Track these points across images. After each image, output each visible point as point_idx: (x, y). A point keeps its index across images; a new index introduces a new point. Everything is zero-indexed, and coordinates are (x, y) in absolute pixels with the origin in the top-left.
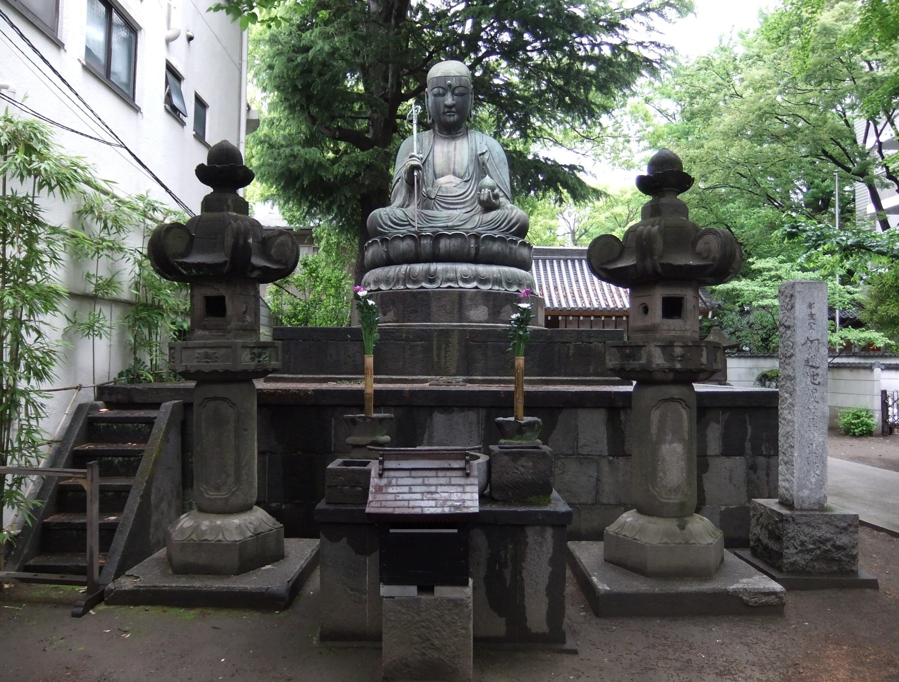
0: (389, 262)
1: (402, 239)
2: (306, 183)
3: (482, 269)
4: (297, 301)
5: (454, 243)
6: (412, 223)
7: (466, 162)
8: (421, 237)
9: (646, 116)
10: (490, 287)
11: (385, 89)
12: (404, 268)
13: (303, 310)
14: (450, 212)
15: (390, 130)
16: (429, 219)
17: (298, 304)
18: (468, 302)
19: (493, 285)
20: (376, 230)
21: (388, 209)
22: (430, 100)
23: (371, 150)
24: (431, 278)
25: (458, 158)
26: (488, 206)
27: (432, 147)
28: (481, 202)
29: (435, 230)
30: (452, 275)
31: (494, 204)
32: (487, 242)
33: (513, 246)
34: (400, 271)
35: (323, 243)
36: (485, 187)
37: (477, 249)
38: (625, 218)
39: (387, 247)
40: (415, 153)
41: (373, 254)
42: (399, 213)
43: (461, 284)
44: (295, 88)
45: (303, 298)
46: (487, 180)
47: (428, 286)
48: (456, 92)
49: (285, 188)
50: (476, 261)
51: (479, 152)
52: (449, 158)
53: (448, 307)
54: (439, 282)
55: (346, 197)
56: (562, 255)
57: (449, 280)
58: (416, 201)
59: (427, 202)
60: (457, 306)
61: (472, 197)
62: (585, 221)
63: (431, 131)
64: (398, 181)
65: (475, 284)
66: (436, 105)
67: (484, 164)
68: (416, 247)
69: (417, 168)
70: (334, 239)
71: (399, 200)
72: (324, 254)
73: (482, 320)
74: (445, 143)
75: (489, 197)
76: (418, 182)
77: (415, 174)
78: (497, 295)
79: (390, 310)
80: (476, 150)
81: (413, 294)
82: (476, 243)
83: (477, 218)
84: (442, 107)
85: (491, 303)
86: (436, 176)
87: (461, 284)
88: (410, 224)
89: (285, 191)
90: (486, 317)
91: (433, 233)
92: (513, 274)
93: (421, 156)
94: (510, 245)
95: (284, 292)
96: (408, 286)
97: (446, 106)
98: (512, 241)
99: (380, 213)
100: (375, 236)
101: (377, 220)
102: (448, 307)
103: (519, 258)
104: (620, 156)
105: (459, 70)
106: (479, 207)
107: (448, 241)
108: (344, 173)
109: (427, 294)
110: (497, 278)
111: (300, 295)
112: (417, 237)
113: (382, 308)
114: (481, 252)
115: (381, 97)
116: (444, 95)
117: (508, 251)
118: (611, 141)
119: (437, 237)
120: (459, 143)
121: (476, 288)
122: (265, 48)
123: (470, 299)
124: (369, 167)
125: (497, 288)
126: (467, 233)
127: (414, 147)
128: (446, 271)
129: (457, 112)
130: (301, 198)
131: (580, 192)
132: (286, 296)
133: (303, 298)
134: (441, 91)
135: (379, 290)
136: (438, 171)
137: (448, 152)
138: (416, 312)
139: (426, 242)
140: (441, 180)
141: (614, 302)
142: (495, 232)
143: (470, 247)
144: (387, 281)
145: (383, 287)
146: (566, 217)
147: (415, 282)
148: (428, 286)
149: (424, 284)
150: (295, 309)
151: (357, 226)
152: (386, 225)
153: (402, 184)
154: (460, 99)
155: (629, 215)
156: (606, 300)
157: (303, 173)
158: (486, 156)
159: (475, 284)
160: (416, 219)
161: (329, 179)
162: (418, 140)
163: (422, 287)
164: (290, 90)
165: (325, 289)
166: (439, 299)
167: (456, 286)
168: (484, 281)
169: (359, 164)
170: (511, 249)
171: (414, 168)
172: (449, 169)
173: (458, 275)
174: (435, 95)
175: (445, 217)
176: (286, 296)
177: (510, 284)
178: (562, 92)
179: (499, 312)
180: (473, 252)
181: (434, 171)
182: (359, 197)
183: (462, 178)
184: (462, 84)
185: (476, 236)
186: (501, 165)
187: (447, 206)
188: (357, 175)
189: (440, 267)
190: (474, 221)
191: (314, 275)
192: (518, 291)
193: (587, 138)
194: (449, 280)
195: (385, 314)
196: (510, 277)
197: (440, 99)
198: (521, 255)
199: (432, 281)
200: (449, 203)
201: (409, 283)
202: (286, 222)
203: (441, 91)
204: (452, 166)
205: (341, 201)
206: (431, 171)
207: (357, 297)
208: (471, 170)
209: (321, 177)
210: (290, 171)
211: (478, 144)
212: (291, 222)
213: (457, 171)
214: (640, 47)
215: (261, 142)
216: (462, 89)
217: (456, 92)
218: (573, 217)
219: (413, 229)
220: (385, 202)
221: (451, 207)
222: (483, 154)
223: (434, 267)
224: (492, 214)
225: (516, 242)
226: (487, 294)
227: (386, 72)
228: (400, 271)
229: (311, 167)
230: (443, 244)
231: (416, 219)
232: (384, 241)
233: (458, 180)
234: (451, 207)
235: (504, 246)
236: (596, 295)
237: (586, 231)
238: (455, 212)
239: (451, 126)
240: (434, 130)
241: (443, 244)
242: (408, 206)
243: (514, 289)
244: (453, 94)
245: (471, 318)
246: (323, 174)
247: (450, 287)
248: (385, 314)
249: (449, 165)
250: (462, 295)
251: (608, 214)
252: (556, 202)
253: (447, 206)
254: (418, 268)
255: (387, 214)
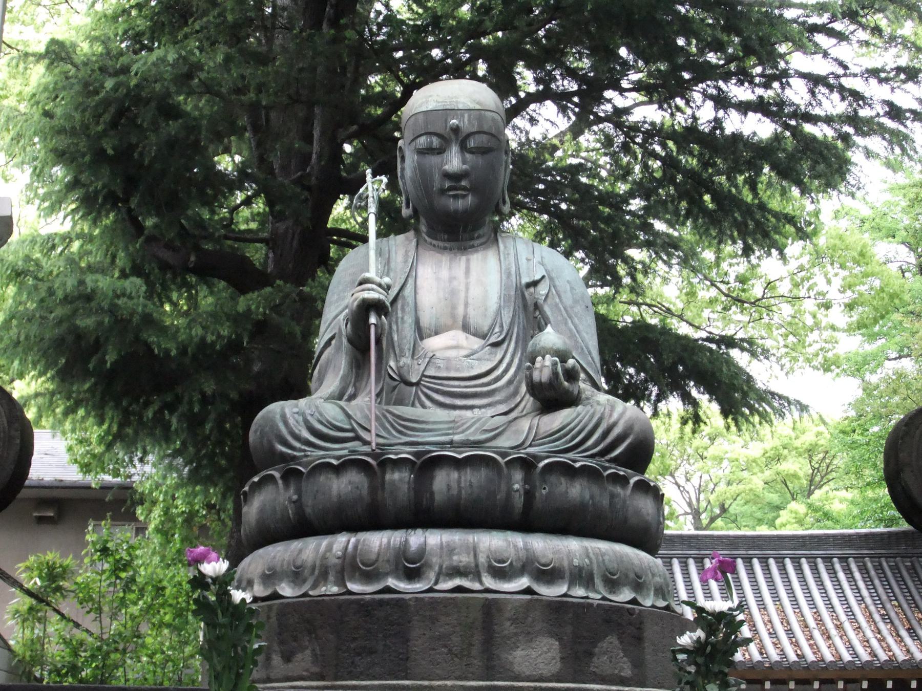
0: (302, 527)
1: (337, 470)
2: (111, 358)
3: (543, 546)
4: (79, 635)
5: (472, 478)
6: (362, 433)
7: (493, 302)
8: (386, 464)
9: (862, 254)
10: (563, 589)
11: (305, 159)
12: (341, 542)
13: (93, 657)
14: (457, 412)
15: (314, 250)
16: (405, 425)
17: (81, 643)
18: (508, 628)
19: (571, 585)
20: (272, 450)
21: (302, 402)
22: (408, 165)
23: (268, 289)
24: (411, 566)
25: (475, 292)
26: (552, 396)
27: (413, 268)
28: (535, 389)
29: (421, 448)
30: (463, 559)
31: (567, 392)
32: (553, 479)
33: (619, 490)
34: (329, 548)
35: (157, 512)
36: (543, 353)
37: (529, 495)
38: (805, 482)
39: (299, 492)
40: (372, 274)
41: (262, 511)
42: (332, 412)
43: (489, 582)
44: (100, 156)
45: (94, 628)
46: (549, 337)
47: (402, 585)
48: (471, 143)
49: (64, 376)
50: (526, 524)
51: (525, 280)
52: (453, 293)
53: (456, 639)
54: (432, 576)
55: (203, 394)
56: (690, 547)
57: (457, 572)
58: (373, 387)
59: (398, 388)
60: (477, 638)
61: (510, 382)
62: (722, 487)
63: (411, 234)
64: (328, 343)
65: (524, 582)
66: (423, 174)
67: (536, 306)
68: (373, 490)
69: (378, 307)
70: (181, 506)
71: (332, 384)
72: (157, 540)
73: (546, 671)
74: (445, 258)
75: (555, 374)
76: (378, 341)
77: (373, 320)
78: (583, 609)
79: (303, 649)
80: (518, 275)
81: (364, 607)
82: (526, 480)
83: (525, 424)
84: (437, 177)
85: (569, 629)
86: (421, 333)
87: (489, 582)
88: (358, 438)
89: (63, 380)
90: (555, 667)
91: (415, 454)
92: (620, 559)
93: (386, 280)
94: (611, 488)
95: (50, 613)
96: (353, 587)
97: (447, 176)
98: (615, 478)
99: (284, 413)
100: (267, 467)
101: (274, 426)
102: (456, 639)
103: (633, 520)
104: (809, 340)
105: (477, 97)
106: (529, 402)
107: (455, 475)
108: (203, 339)
109: (401, 606)
110: (580, 569)
111: (88, 621)
112: (376, 466)
113: (282, 643)
114: (538, 503)
115: (298, 182)
116: (440, 151)
117: (605, 502)
118: (787, 310)
119: (427, 465)
120: (476, 259)
121: (528, 591)
122: (38, 74)
123: (514, 620)
124: (261, 328)
125: (580, 592)
126: (503, 455)
127: (367, 268)
128: (450, 550)
129: (472, 190)
130: (102, 399)
131: (738, 398)
132: (54, 626)
133: (95, 628)
134: (436, 141)
135: (276, 596)
136: (426, 320)
137: (452, 279)
138: (371, 652)
139: (398, 478)
140: (433, 343)
141: (815, 647)
142: (571, 455)
143: (510, 491)
144: (296, 575)
145: (287, 590)
146: (682, 481)
147: (369, 577)
148: (402, 585)
149: (391, 582)
150: (76, 654)
151: (228, 458)
152: (297, 438)
153: (338, 348)
154: (480, 160)
155: (812, 477)
156: (796, 644)
157: (107, 339)
158: (542, 289)
159: (524, 582)
160: (373, 426)
161: (167, 352)
162: (379, 253)
163: (388, 590)
164: (87, 158)
165: (148, 610)
166: (433, 620)
167: (477, 586)
168: (549, 575)
169: (237, 319)
170: (613, 496)
171: (367, 307)
172: (453, 316)
173: (482, 559)
174: (422, 152)
175: (439, 425)
176: (54, 626)
177: (613, 584)
178: (696, 184)
179: (590, 654)
180: (518, 501)
181: (417, 322)
182: (234, 395)
183: (484, 337)
184: (486, 128)
185: (527, 464)
186: (579, 309)
187: (448, 400)
188: (234, 346)
189: (434, 539)
190: (517, 432)
191: (123, 575)
192: (634, 601)
193: (738, 301)
194: (457, 572)
195: (288, 658)
196: (613, 566)
197: (434, 160)
198: (638, 513)
199: (412, 575)
200: (455, 392)
201: (352, 579)
202: (76, 467)
203: (436, 141)
204: (460, 310)
205: (191, 403)
206: (409, 320)
207: (200, 581)
208: (507, 318)
209: (148, 347)
210: (79, 335)
211: (523, 262)
212: (86, 468)
213: (472, 322)
214: (873, 82)
215: (18, 274)
216: (484, 138)
217: (471, 143)
218: (695, 481)
219: (366, 449)
220: (298, 388)
221: (459, 402)
222: (535, 284)
223: (416, 539)
224: (562, 417)
225: (624, 481)
226: (558, 607)
227: (308, 122)
228: (329, 548)
229: (130, 328)
230: (444, 482)
231: (373, 426)
232: (291, 475)
233: (476, 343)
234: (459, 402)
235: (596, 490)
236: (773, 634)
237: (724, 510)
238: (468, 414)
239: (458, 226)
240: (417, 231)
241: (444, 482)
242: (352, 397)
243: (625, 595)
244: (463, 148)
245: (517, 668)
246: (153, 339)
247: (459, 589)
248: (288, 658)
249: (454, 307)
250: (491, 608)
251: (768, 474)
252: (684, 422)
253: (448, 400)
254: (377, 541)
255: (302, 414)
